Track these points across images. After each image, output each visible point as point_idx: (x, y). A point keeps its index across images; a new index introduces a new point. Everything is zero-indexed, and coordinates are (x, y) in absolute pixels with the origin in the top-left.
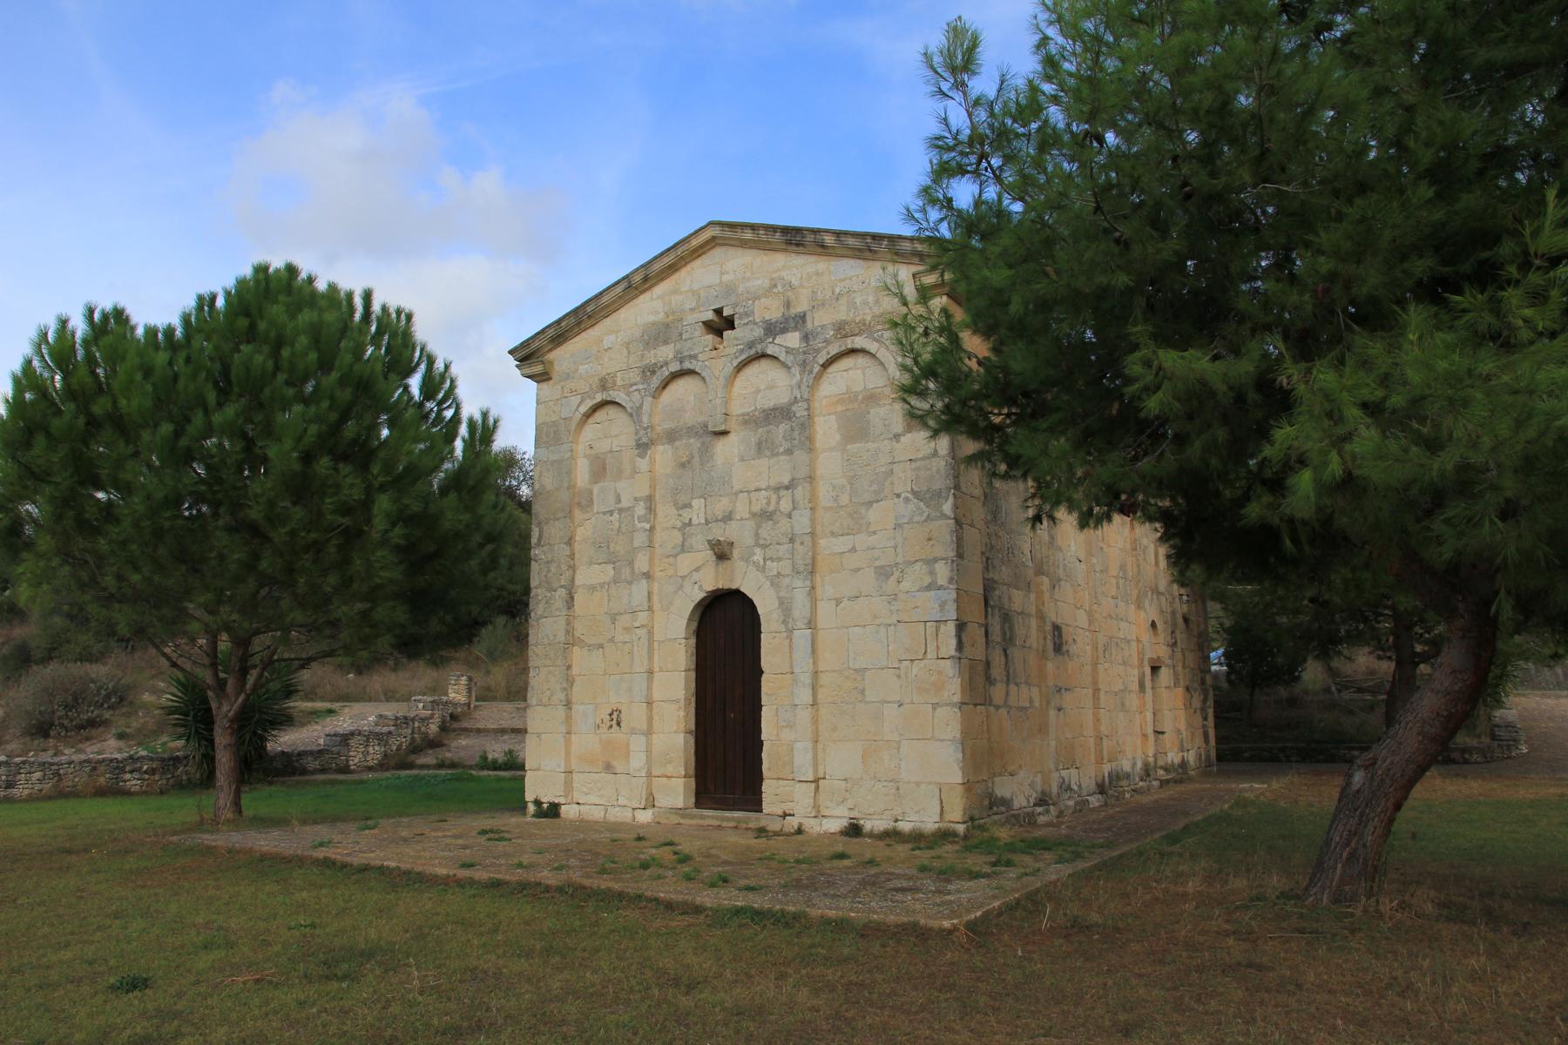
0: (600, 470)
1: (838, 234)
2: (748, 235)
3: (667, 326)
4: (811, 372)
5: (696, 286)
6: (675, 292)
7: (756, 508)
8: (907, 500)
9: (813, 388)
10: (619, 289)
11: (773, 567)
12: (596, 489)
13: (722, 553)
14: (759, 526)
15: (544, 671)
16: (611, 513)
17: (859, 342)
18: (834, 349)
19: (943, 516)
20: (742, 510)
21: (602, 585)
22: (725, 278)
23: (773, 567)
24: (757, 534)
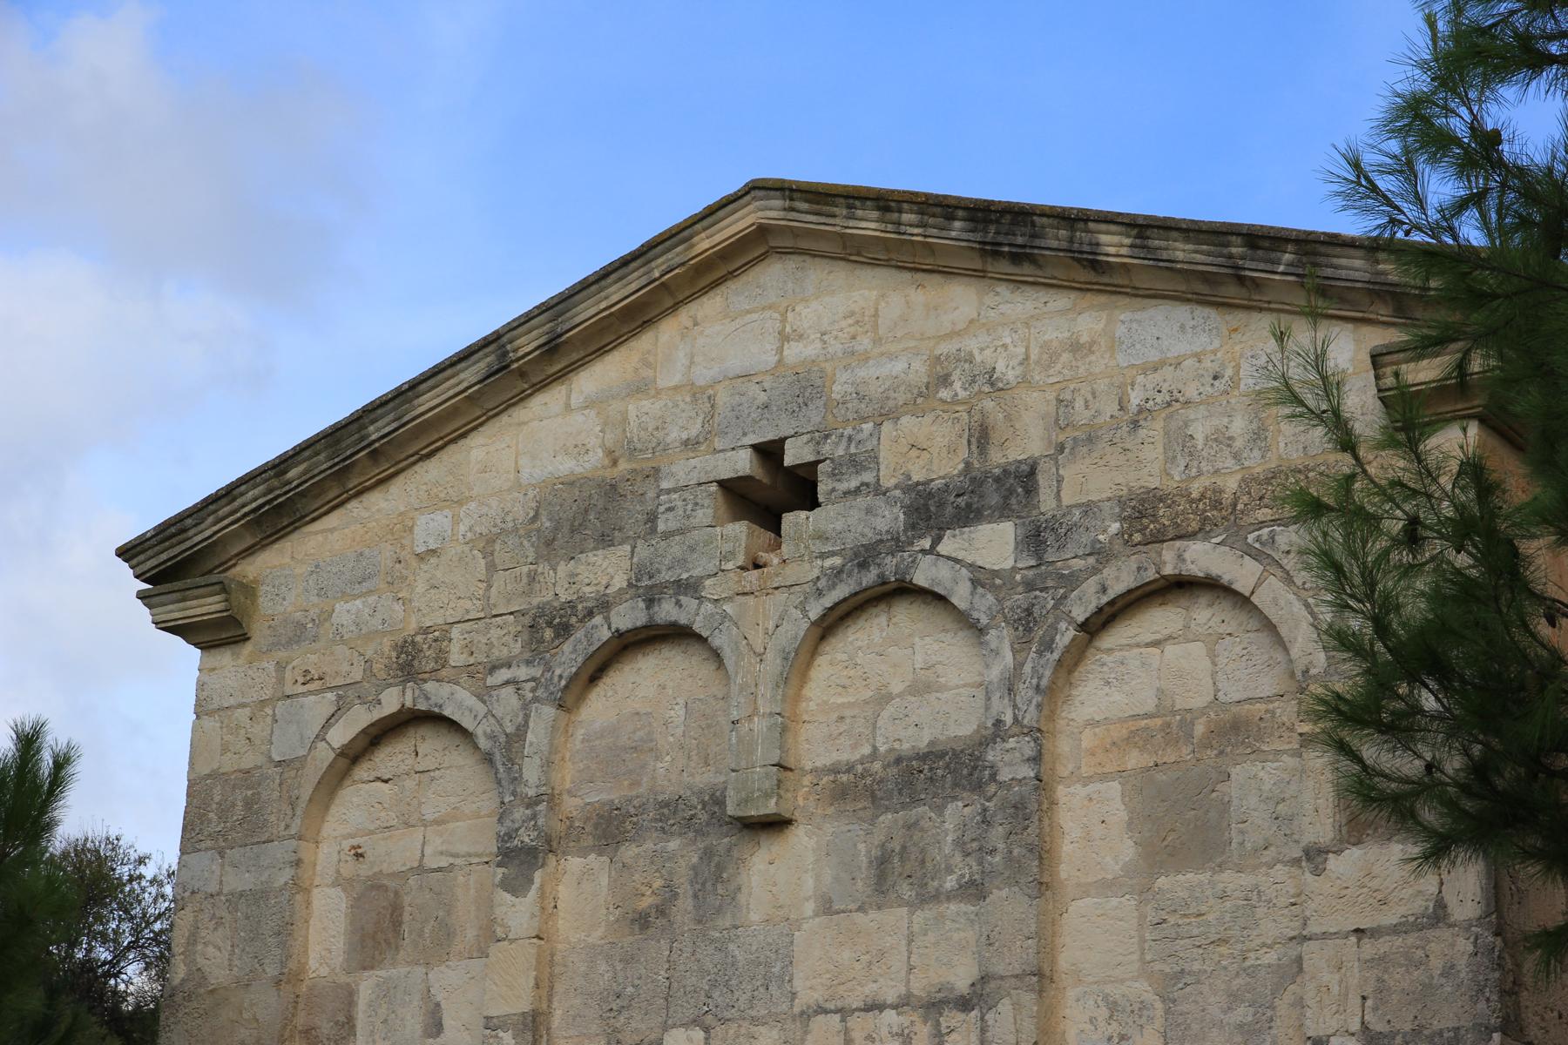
1: (1142, 228)
2: (868, 225)
4: (1047, 646)
5: (702, 375)
6: (640, 388)
9: (1052, 693)
17: (1201, 557)
18: (1122, 578)
22: (795, 352)
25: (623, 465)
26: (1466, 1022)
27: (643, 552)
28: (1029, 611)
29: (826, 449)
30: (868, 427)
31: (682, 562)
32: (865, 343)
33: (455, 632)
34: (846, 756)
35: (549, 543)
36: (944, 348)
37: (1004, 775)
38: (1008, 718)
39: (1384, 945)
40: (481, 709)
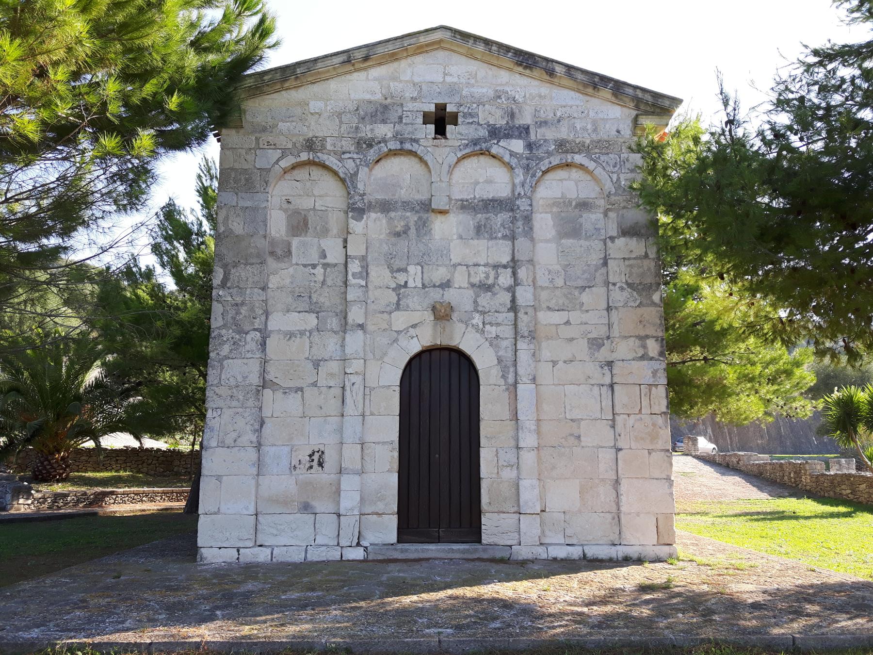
0: (300, 224)
1: (570, 68)
2: (481, 47)
3: (386, 107)
4: (534, 175)
5: (417, 79)
6: (395, 79)
7: (475, 280)
8: (622, 289)
9: (534, 188)
10: (337, 60)
11: (492, 331)
12: (295, 242)
13: (442, 314)
14: (478, 296)
15: (227, 413)
16: (314, 266)
17: (579, 158)
18: (556, 160)
19: (654, 304)
20: (460, 278)
21: (302, 333)
22: (448, 79)
23: (492, 331)
24: (475, 302)
25: (389, 100)
26: (653, 282)
27: (398, 127)
28: (528, 165)
29: (461, 109)
30: (475, 105)
31: (413, 133)
32: (473, 81)
33: (328, 139)
34: (465, 197)
35: (363, 119)
36: (498, 88)
37: (522, 208)
38: (523, 193)
39: (631, 262)
40: (341, 165)
